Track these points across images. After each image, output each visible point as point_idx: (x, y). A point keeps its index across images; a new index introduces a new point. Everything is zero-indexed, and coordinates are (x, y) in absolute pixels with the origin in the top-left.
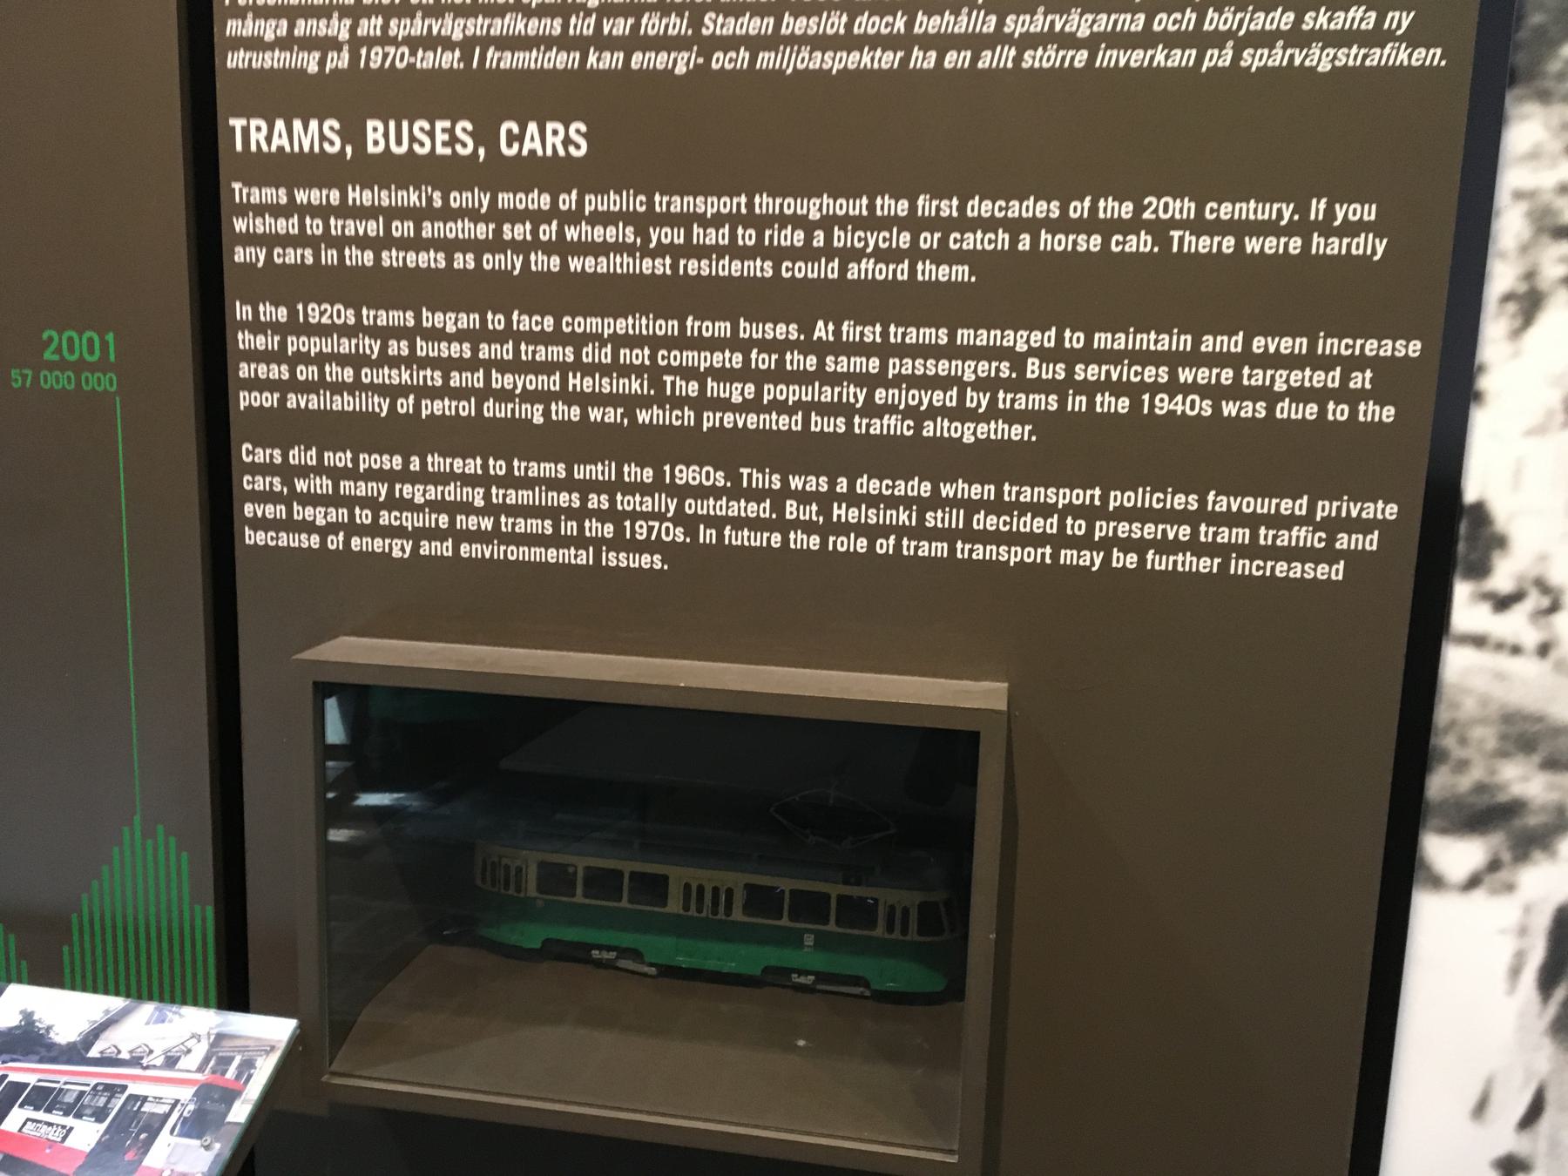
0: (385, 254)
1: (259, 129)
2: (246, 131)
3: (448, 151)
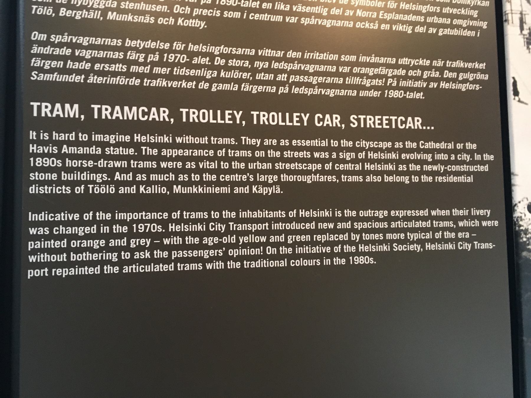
0: (340, 154)
2: (100, 110)
3: (380, 127)
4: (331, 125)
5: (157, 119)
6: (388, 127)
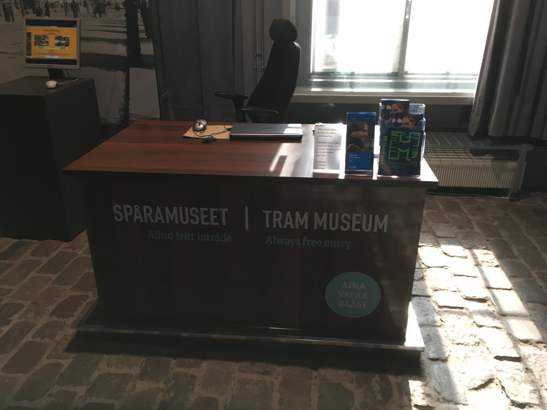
1: (278, 216)
3: (208, 224)
4: (163, 222)
5: (163, 222)
6: (217, 224)
